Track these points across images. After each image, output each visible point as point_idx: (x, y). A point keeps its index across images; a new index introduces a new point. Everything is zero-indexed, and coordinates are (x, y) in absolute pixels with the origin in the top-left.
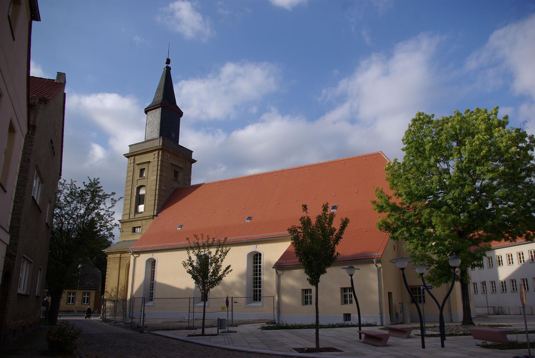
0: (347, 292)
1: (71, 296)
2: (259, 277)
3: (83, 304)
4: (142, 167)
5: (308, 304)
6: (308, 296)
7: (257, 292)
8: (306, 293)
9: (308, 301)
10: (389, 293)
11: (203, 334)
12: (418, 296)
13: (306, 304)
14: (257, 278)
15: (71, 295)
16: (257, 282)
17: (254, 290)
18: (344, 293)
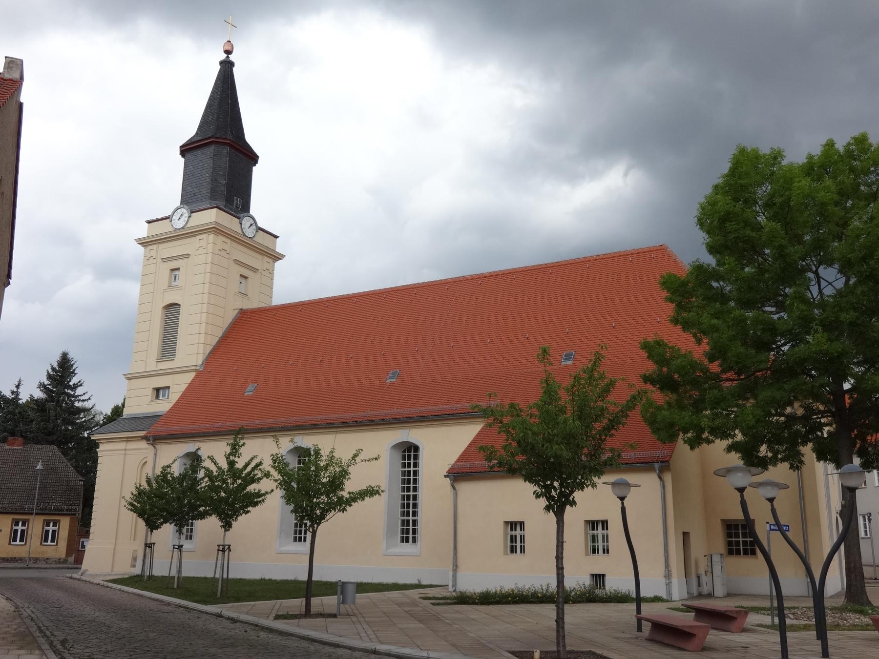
0: (597, 530)
1: (20, 528)
2: (413, 495)
3: (12, 543)
4: (174, 264)
5: (516, 552)
6: (516, 536)
7: (408, 525)
8: (512, 530)
9: (516, 546)
10: (684, 533)
11: (308, 613)
12: (741, 537)
13: (512, 552)
14: (409, 496)
15: (18, 526)
16: (408, 505)
17: (403, 521)
18: (591, 532)
